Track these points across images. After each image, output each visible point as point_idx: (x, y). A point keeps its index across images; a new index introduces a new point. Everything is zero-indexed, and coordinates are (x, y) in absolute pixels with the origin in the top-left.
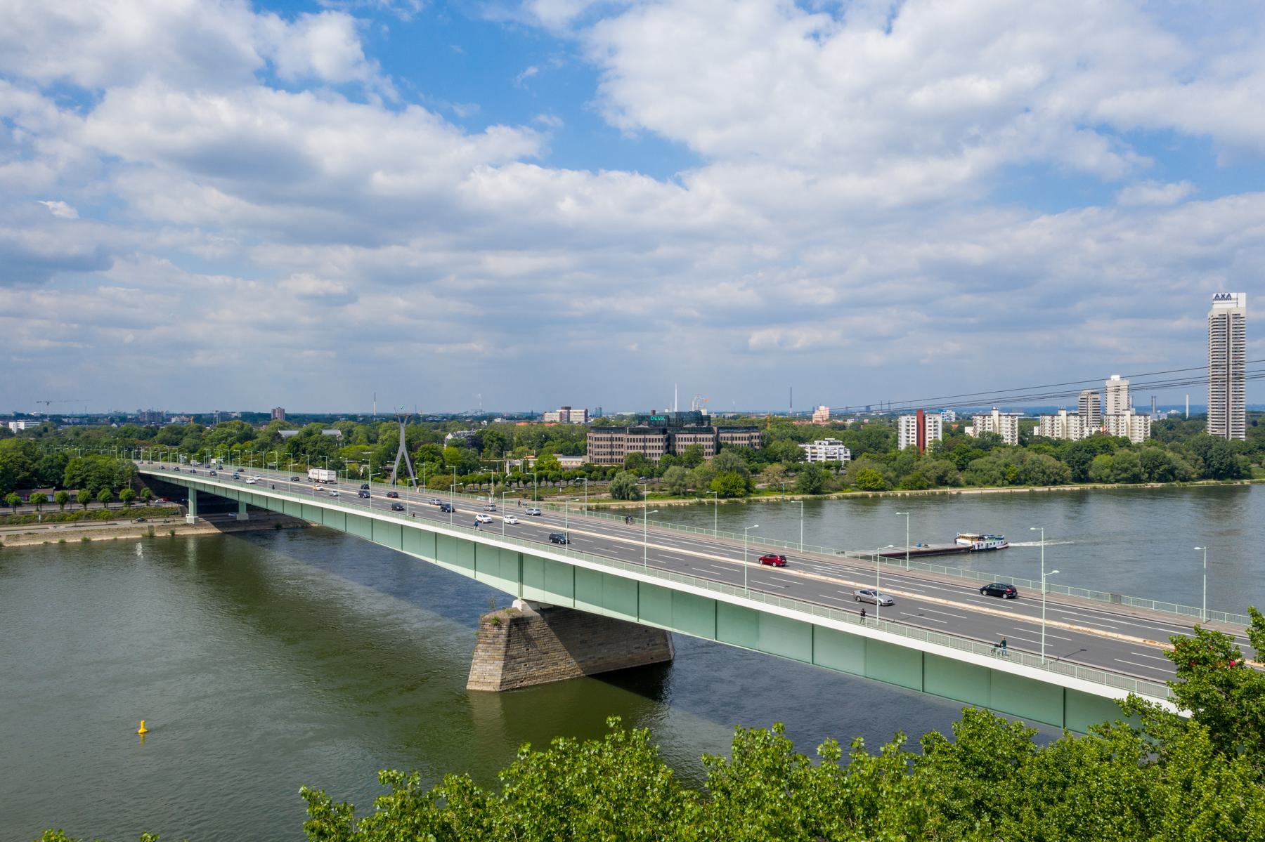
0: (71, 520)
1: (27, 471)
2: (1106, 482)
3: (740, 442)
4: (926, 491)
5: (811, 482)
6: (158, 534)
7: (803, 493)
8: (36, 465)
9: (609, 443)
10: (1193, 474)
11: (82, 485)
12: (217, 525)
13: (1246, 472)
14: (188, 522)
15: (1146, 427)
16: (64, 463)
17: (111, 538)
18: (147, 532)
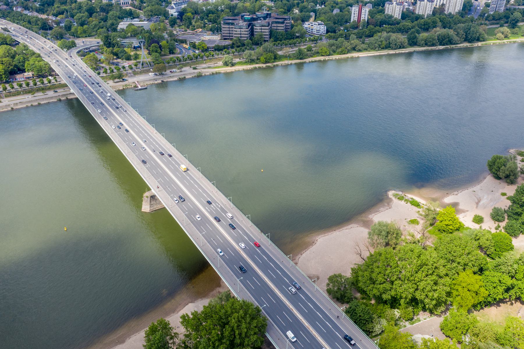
1: (12, 66)
6: (62, 99)
8: (14, 63)
9: (228, 29)
14: (71, 92)
16: (24, 60)
18: (58, 98)
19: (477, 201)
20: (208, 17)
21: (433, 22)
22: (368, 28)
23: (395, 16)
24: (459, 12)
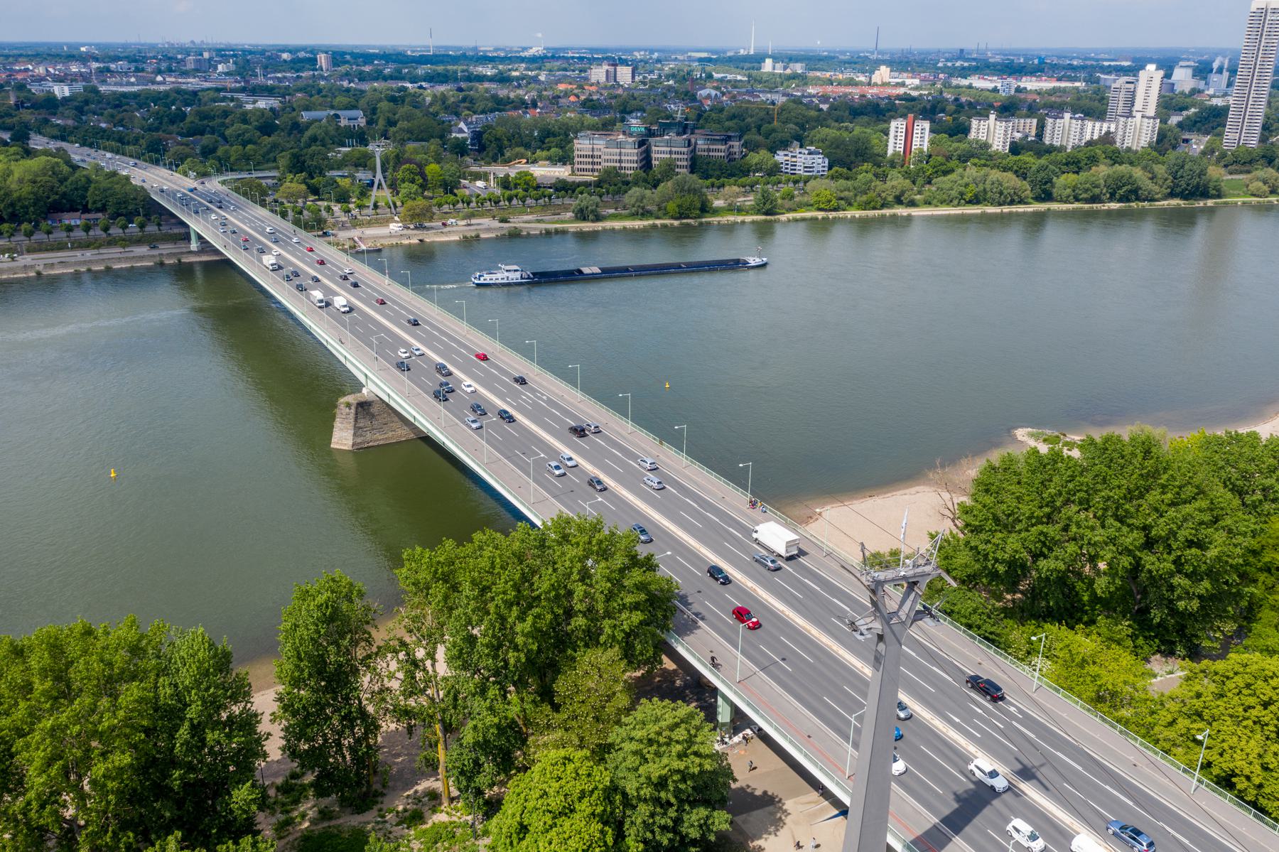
2: (1065, 202)
3: (717, 154)
4: (880, 212)
5: (765, 204)
6: (167, 262)
7: (757, 214)
8: (63, 189)
10: (1157, 194)
13: (1214, 192)
15: (1153, 131)
18: (158, 259)
20: (543, 143)
21: (1088, 158)
22: (931, 163)
23: (995, 148)
24: (1150, 144)
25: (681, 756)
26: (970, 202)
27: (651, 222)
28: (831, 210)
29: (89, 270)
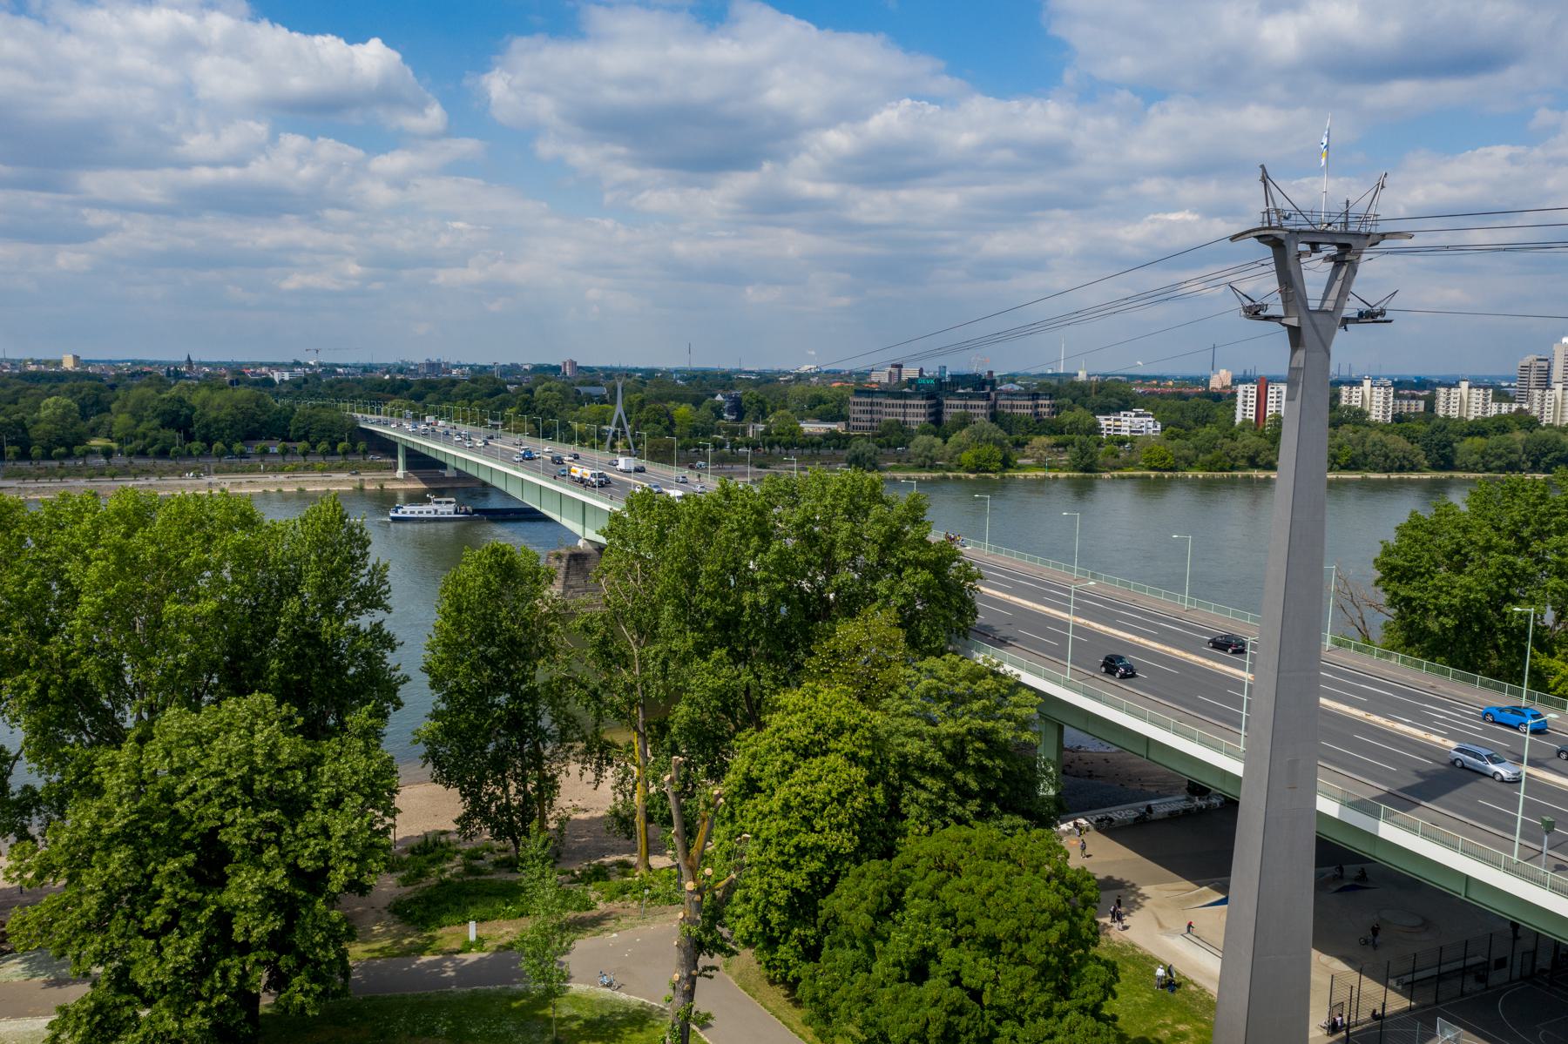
0: (289, 471)
2: (1472, 471)
6: (367, 487)
8: (264, 418)
9: (869, 408)
11: (305, 437)
12: (424, 480)
17: (324, 489)
18: (357, 485)
19: (1520, 933)
23: (1373, 418)
25: (987, 713)
26: (1346, 468)
27: (941, 474)
28: (1166, 470)
29: (280, 491)
